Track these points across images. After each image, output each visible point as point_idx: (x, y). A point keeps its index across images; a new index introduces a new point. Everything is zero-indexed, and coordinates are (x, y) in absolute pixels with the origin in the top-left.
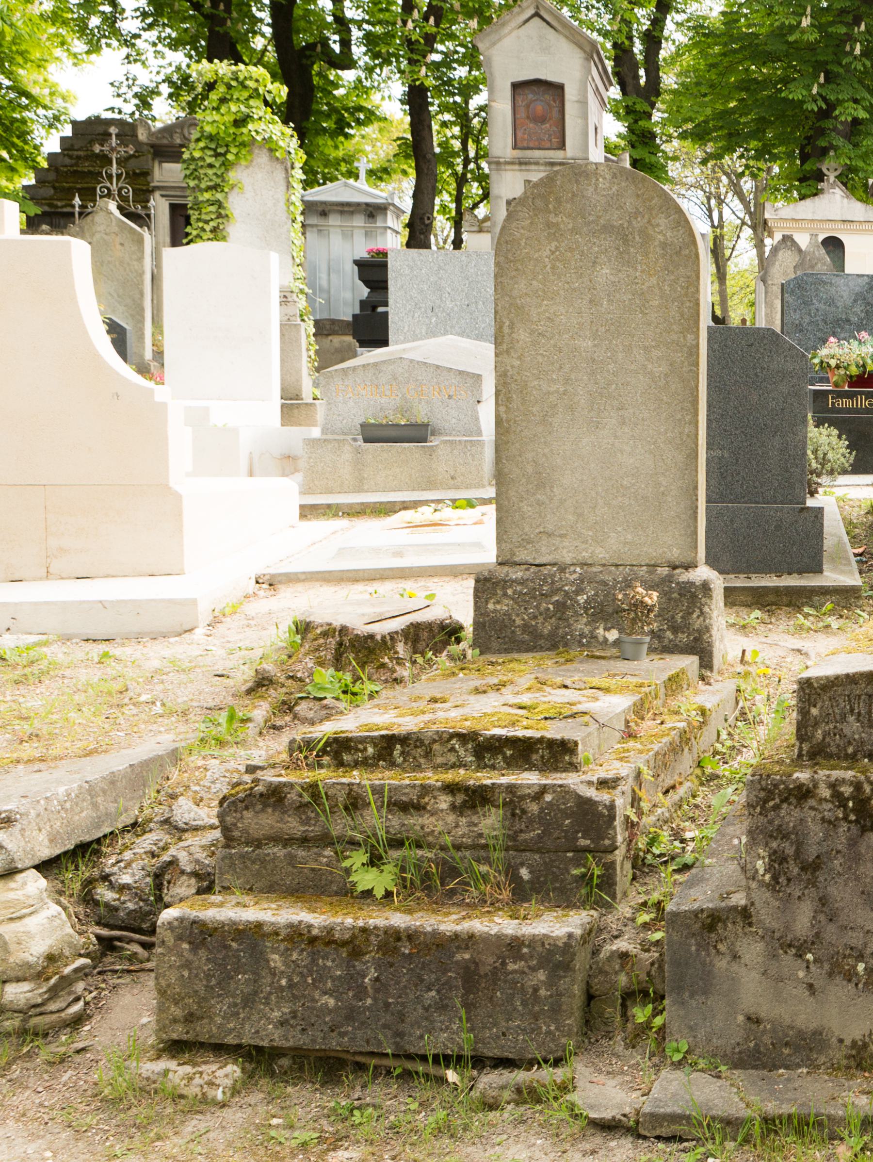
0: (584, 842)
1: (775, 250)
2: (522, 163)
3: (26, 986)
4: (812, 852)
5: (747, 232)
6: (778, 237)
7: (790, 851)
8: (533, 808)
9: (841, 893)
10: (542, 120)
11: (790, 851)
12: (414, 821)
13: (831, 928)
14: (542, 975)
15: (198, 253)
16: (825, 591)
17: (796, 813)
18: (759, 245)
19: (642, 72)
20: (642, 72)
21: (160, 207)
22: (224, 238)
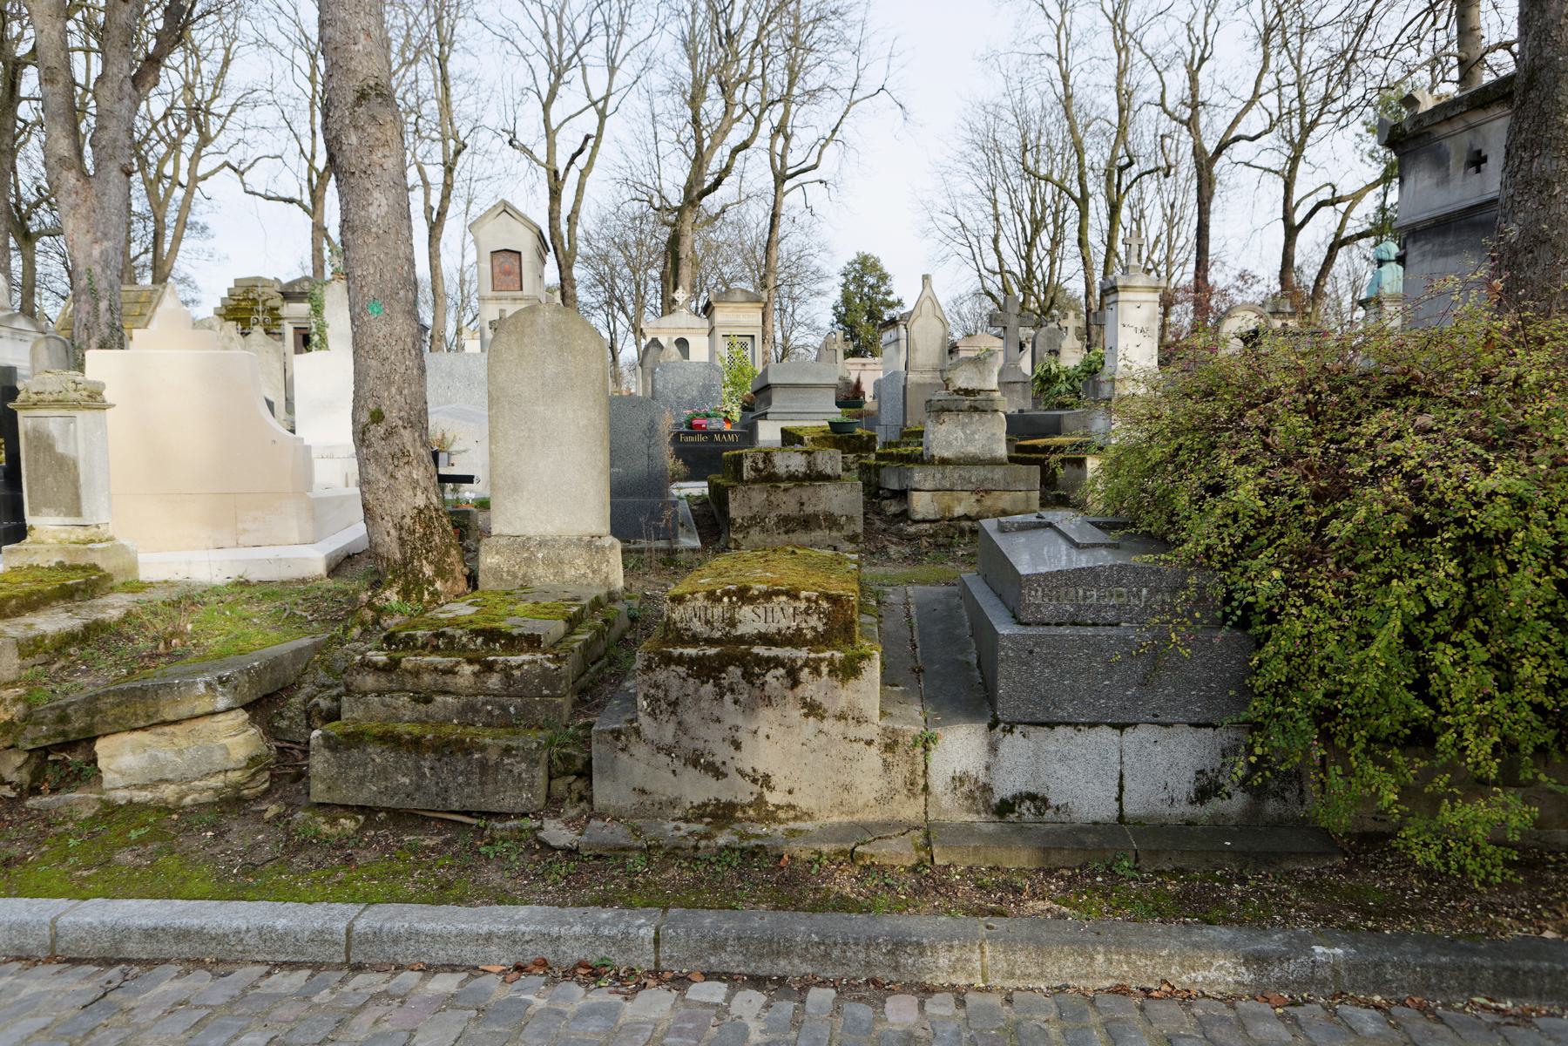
0: (546, 692)
1: (647, 347)
2: (497, 299)
3: (238, 773)
4: (673, 696)
5: (631, 336)
6: (649, 339)
7: (661, 694)
8: (517, 673)
9: (691, 718)
10: (508, 273)
11: (661, 694)
12: (449, 679)
13: (685, 738)
14: (524, 766)
15: (314, 356)
16: (441, 206)
17: (665, 674)
18: (637, 344)
19: (1530, 964)
20: (1530, 964)
21: (289, 330)
22: (327, 348)
